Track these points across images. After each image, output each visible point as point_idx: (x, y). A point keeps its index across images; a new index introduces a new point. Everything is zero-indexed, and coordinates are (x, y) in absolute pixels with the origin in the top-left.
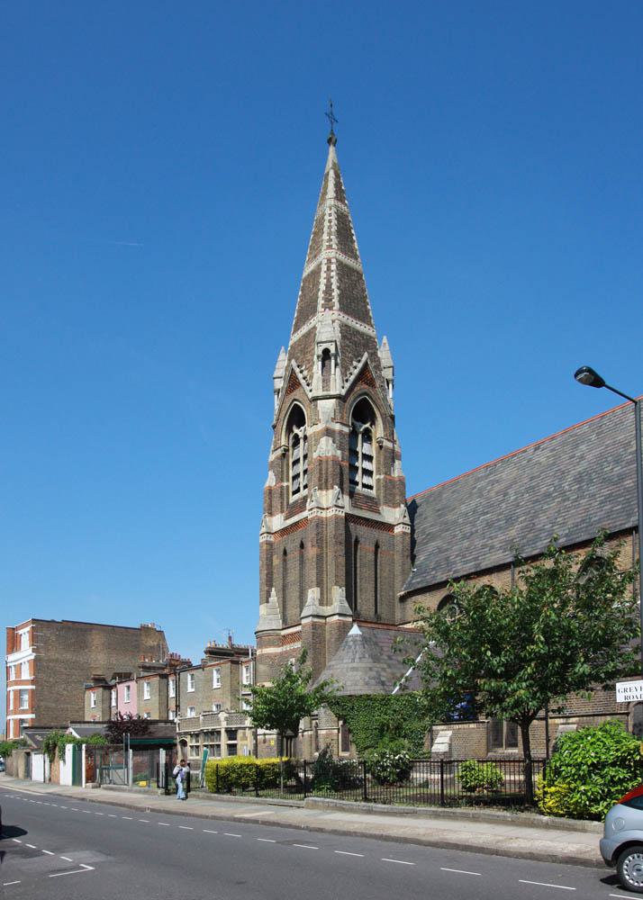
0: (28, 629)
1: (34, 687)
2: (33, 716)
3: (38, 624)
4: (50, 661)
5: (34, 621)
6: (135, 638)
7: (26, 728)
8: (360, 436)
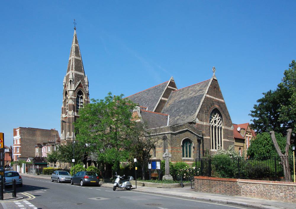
0: (19, 130)
1: (20, 146)
2: (20, 154)
3: (21, 129)
4: (25, 139)
5: (20, 128)
6: (49, 133)
7: (18, 158)
8: (80, 98)
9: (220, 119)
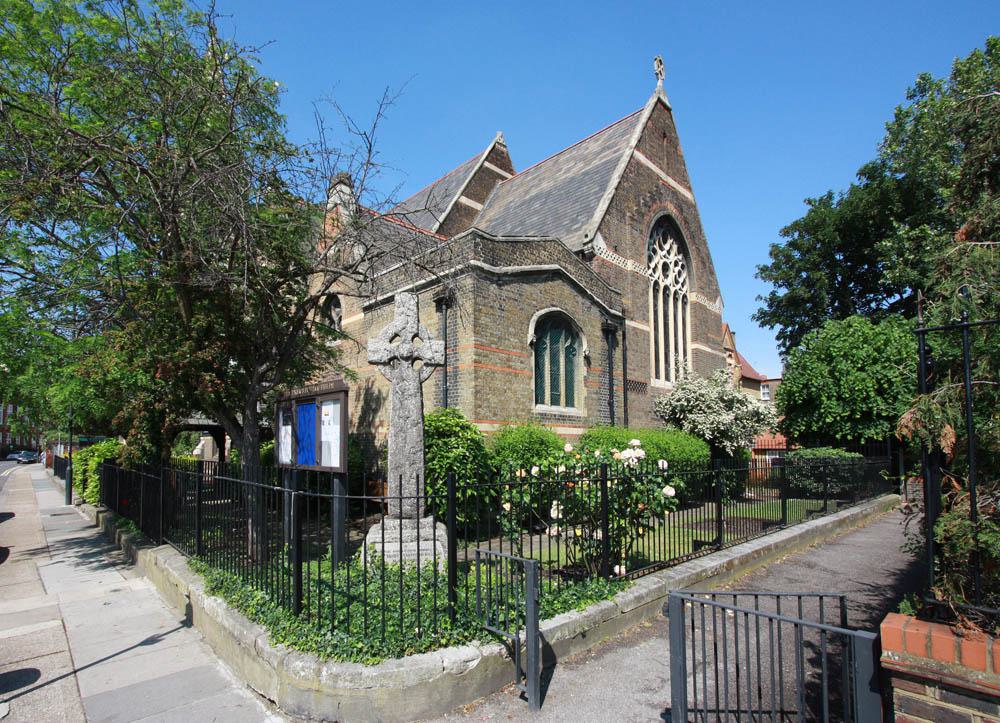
9: (680, 263)
